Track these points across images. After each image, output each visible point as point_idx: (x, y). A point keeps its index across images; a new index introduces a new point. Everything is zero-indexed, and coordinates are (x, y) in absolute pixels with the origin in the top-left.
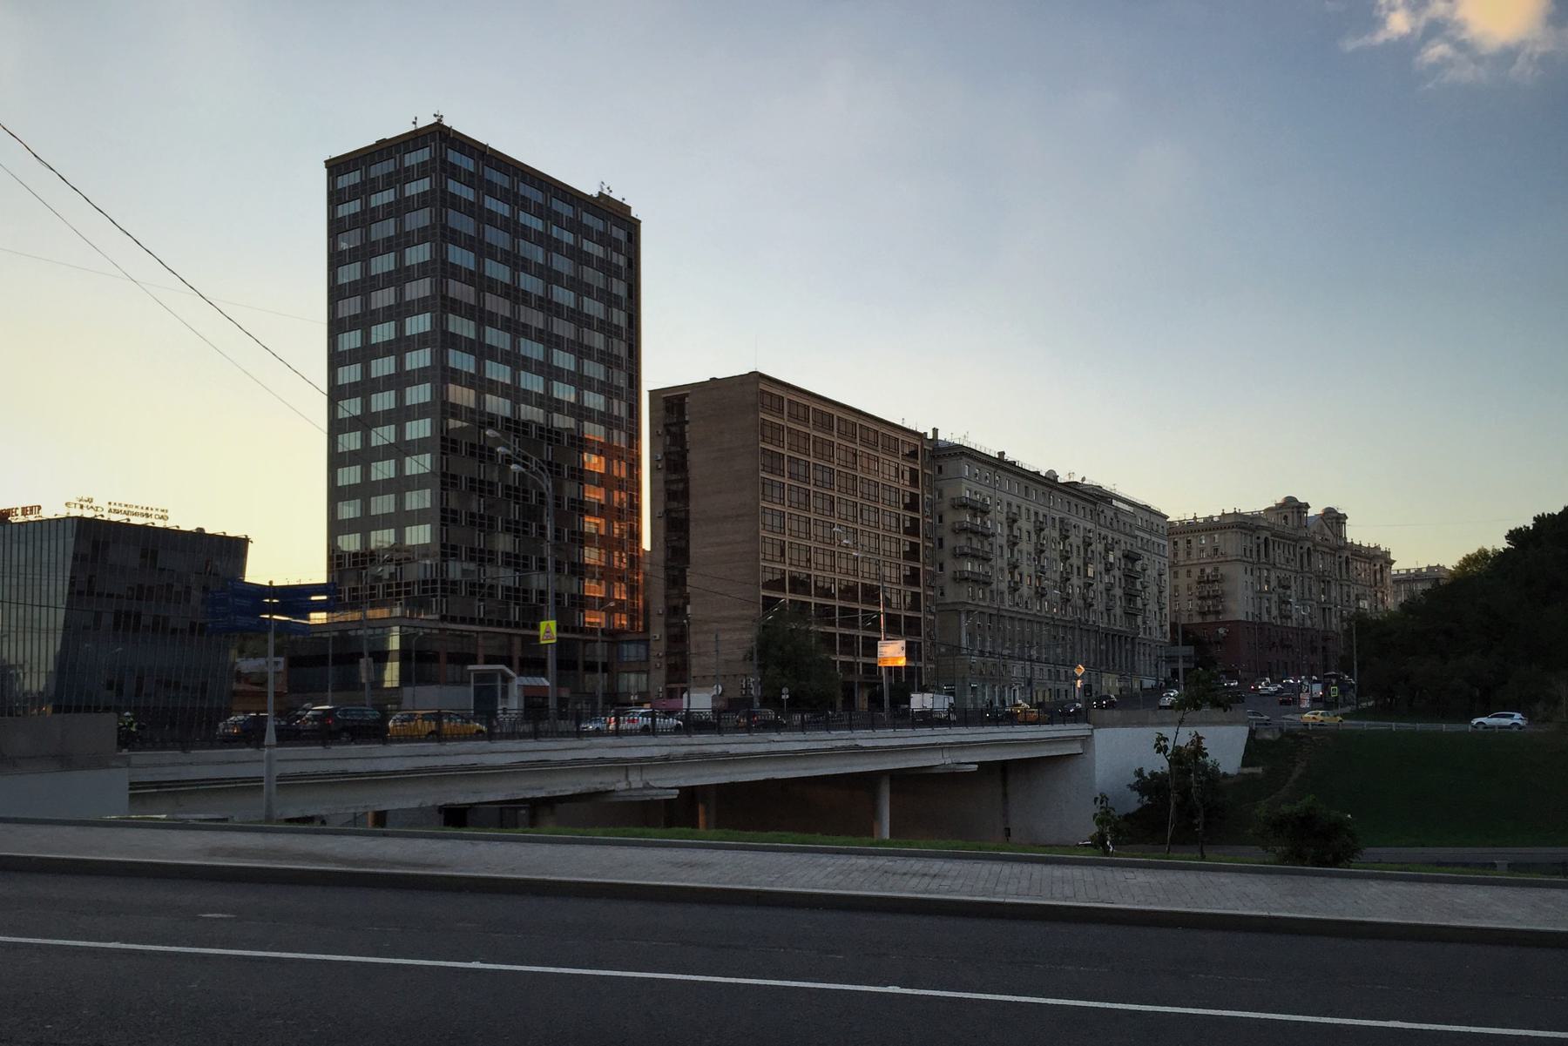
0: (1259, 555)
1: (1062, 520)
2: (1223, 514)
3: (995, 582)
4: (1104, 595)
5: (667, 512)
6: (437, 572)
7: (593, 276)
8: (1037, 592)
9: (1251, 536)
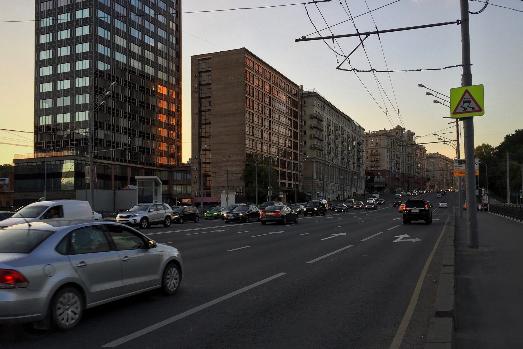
0: (391, 146)
2: (380, 130)
8: (335, 155)
9: (389, 139)
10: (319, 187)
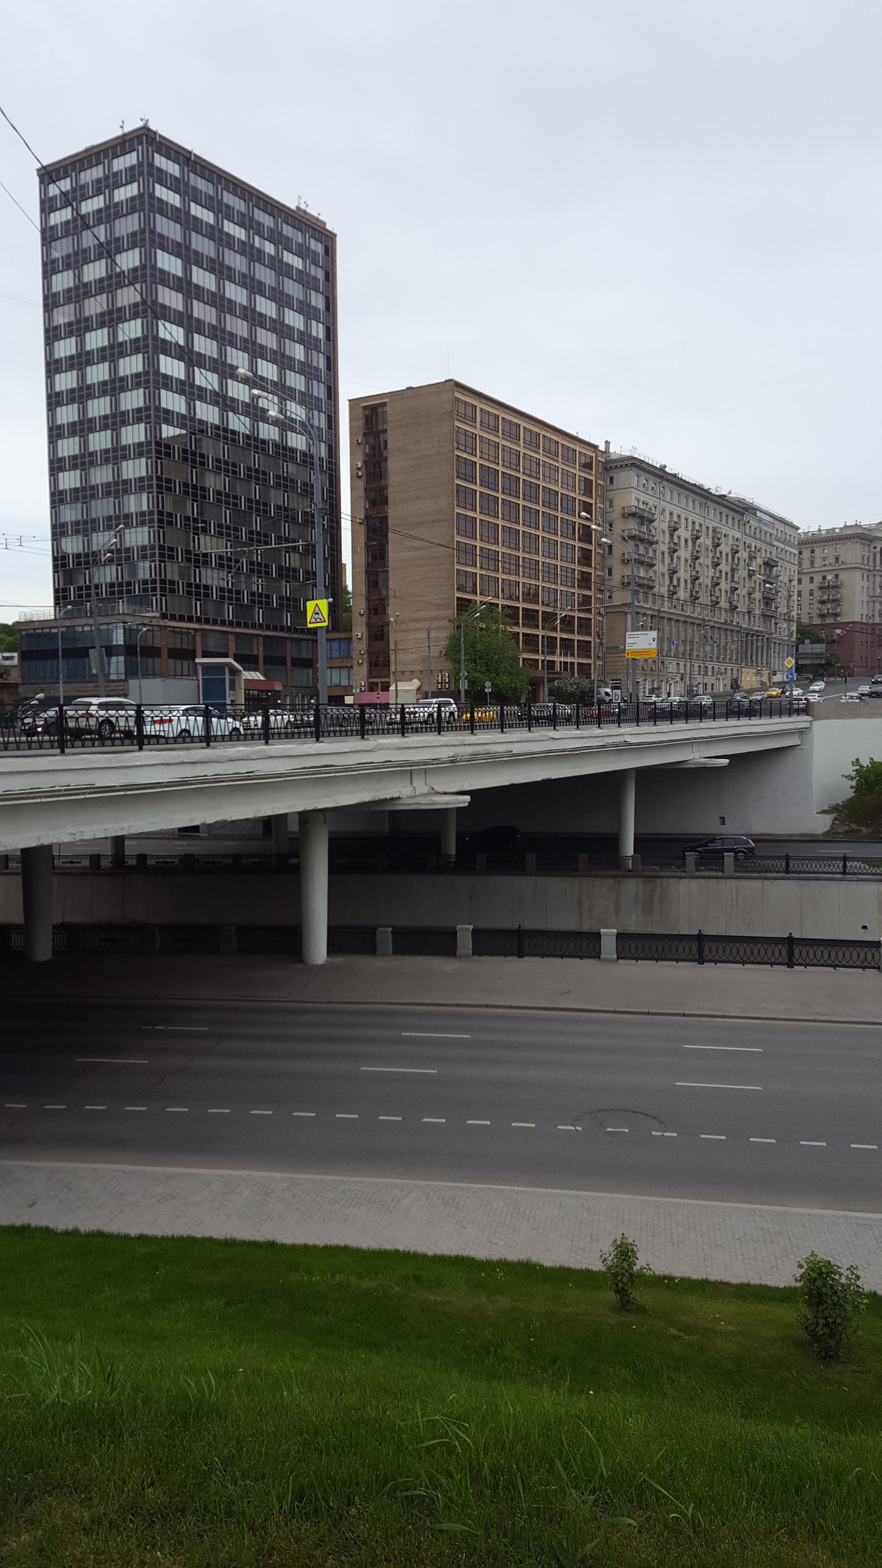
1: (714, 530)
3: (657, 586)
4: (746, 598)
5: (367, 518)
6: (157, 606)
7: (292, 288)
8: (691, 596)
10: (641, 668)
